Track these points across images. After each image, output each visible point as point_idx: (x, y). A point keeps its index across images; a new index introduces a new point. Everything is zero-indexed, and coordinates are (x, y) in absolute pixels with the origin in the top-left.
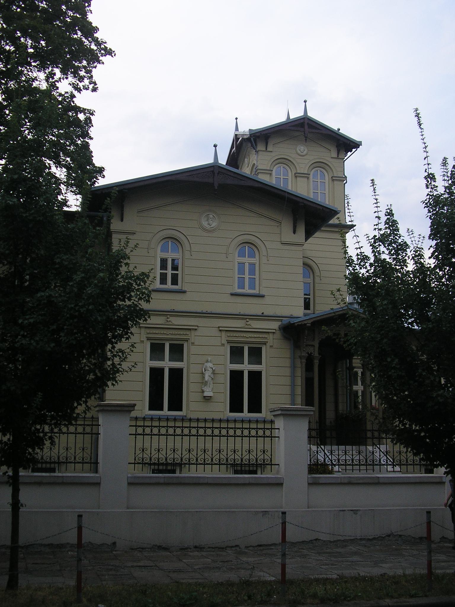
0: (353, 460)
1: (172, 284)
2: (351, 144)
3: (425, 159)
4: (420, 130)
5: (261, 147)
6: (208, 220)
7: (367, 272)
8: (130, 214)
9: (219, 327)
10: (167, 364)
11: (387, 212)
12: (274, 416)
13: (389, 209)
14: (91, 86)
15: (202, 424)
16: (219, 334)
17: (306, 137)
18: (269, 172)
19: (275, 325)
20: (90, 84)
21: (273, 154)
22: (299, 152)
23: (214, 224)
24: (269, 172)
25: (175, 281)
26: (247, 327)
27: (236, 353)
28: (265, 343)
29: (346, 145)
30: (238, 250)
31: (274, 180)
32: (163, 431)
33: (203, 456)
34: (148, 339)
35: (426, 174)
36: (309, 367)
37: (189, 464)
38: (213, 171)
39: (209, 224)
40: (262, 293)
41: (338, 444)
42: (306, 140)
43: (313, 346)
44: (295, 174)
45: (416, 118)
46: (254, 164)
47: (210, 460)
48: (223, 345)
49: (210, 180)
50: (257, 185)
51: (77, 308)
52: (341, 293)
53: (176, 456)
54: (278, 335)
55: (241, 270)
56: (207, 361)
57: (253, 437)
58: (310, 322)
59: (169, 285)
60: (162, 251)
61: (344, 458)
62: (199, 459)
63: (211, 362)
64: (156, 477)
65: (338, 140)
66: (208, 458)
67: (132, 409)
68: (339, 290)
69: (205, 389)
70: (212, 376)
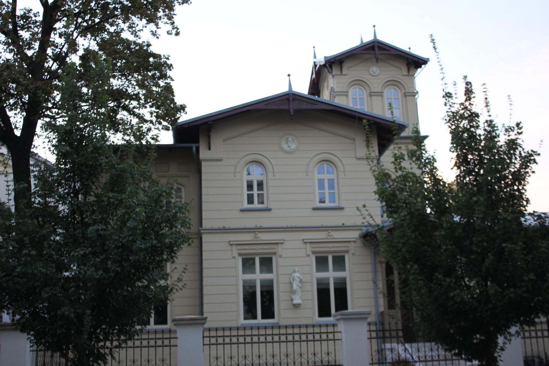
0: (425, 357)
2: (420, 61)
3: (442, 79)
4: (436, 54)
5: (336, 71)
6: (287, 143)
7: (390, 187)
8: (217, 141)
10: (258, 277)
11: (413, 130)
12: (337, 320)
13: (415, 127)
14: (174, 31)
15: (241, 332)
17: (377, 59)
18: (345, 94)
19: (355, 234)
20: (173, 29)
22: (372, 72)
23: (293, 146)
24: (345, 94)
26: (329, 237)
27: (248, 264)
28: (347, 252)
29: (415, 63)
30: (317, 168)
31: (349, 101)
32: (213, 340)
34: (240, 255)
35: (444, 94)
36: (389, 271)
38: (288, 99)
39: (289, 147)
40: (342, 205)
41: (425, 341)
42: (377, 61)
45: (432, 44)
46: (332, 88)
48: (308, 256)
49: (286, 107)
51: (121, 239)
52: (367, 208)
53: (330, 359)
54: (359, 243)
55: (321, 185)
56: (294, 272)
60: (319, 173)
61: (430, 354)
63: (298, 272)
65: (407, 59)
67: (203, 321)
68: (364, 206)
69: (294, 297)
70: (300, 285)
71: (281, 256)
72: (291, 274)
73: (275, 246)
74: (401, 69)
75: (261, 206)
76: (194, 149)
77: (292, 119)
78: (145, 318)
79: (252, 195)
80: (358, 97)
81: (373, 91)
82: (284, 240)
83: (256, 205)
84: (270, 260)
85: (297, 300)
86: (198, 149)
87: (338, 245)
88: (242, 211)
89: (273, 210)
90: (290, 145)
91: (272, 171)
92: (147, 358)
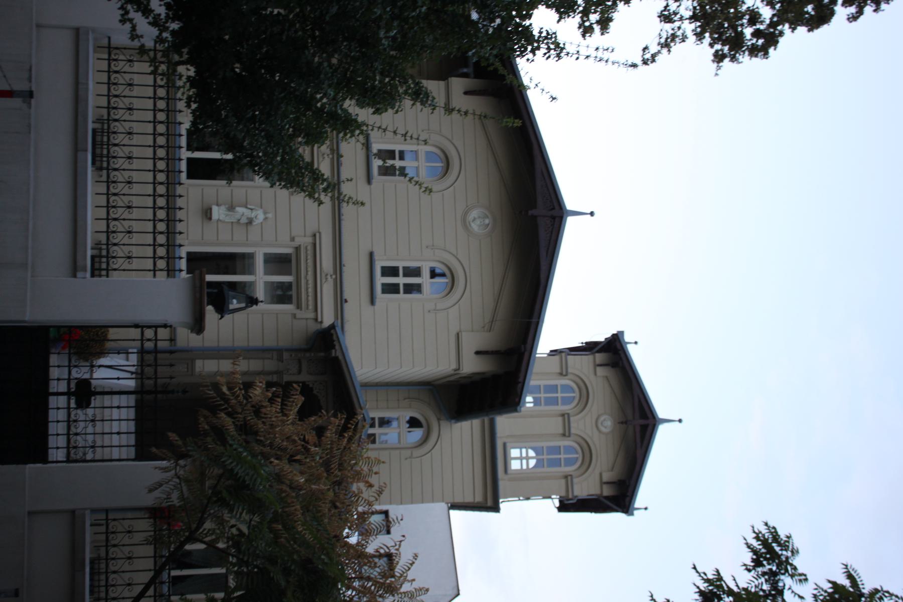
1: (383, 285)
9: (320, 233)
14: (648, 56)
16: (309, 232)
17: (626, 423)
21: (592, 376)
22: (602, 418)
23: (475, 227)
25: (391, 289)
26: (323, 275)
28: (299, 307)
34: (297, 249)
37: (109, 60)
39: (474, 219)
42: (622, 423)
43: (300, 372)
44: (568, 414)
47: (116, 69)
48: (293, 239)
50: (544, 267)
54: (313, 327)
56: (265, 213)
58: (339, 354)
60: (427, 153)
62: (117, 75)
63: (266, 219)
69: (223, 208)
70: (244, 220)
74: (612, 470)
75: (378, 288)
76: (465, 70)
78: (195, 145)
80: (559, 395)
81: (572, 419)
83: (377, 163)
85: (217, 213)
87: (311, 285)
88: (371, 255)
89: (368, 187)
90: (478, 222)
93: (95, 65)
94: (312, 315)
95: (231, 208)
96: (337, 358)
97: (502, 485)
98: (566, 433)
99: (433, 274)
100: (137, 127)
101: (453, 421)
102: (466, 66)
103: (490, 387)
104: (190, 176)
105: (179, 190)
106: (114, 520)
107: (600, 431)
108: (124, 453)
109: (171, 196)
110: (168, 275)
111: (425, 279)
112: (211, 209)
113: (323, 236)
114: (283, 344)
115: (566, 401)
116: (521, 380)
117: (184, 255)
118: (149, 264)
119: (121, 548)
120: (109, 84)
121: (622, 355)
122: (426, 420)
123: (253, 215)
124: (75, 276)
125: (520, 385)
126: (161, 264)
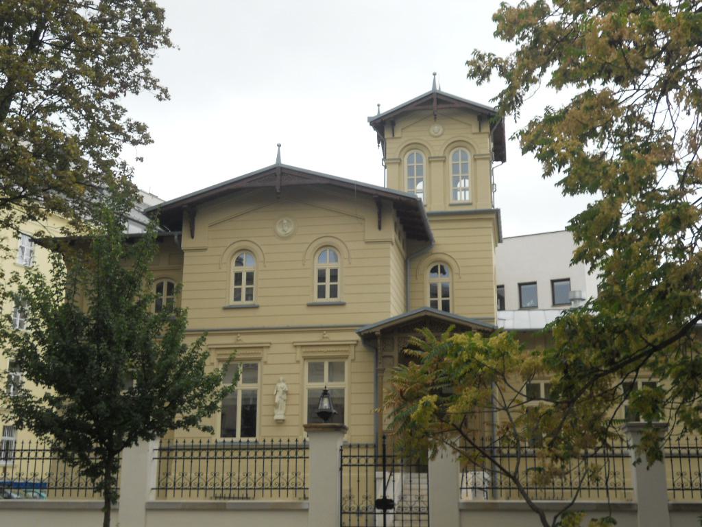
1: (331, 297)
8: (202, 228)
16: (293, 350)
21: (402, 140)
22: (432, 133)
23: (289, 230)
25: (334, 292)
27: (315, 371)
28: (346, 357)
30: (316, 258)
33: (197, 481)
34: (305, 358)
39: (284, 231)
42: (435, 118)
43: (391, 357)
44: (429, 158)
47: (188, 484)
48: (298, 362)
50: (318, 181)
54: (361, 347)
56: (279, 382)
57: (363, 456)
59: (328, 299)
63: (284, 381)
64: (241, 503)
66: (686, 480)
69: (276, 411)
70: (285, 397)
71: (266, 363)
72: (275, 384)
73: (260, 351)
74: (470, 125)
75: (333, 300)
76: (176, 237)
77: (279, 198)
79: (324, 286)
80: (415, 164)
81: (432, 155)
82: (270, 343)
83: (328, 299)
84: (255, 367)
85: (279, 415)
86: (180, 237)
87: (334, 349)
88: (310, 305)
89: (347, 306)
90: (286, 228)
91: (263, 259)
92: (262, 471)
93: (173, 498)
94: (352, 349)
95: (276, 406)
96: (381, 331)
97: (480, 206)
98: (443, 160)
99: (239, 262)
100: (292, 469)
101: (433, 243)
102: (173, 236)
103: (408, 221)
104: (254, 435)
105: (261, 443)
106: (467, 483)
107: (442, 134)
108: (423, 481)
109: (264, 448)
110: (308, 448)
111: (244, 270)
112: (277, 420)
113: (295, 340)
114: (372, 368)
115: (420, 160)
116: (398, 198)
117: (222, 440)
118: (300, 462)
119: (224, 479)
120: (182, 489)
121: (387, 118)
122: (433, 262)
123: (281, 391)
124: (307, 510)
125: (402, 198)
126: (300, 453)
